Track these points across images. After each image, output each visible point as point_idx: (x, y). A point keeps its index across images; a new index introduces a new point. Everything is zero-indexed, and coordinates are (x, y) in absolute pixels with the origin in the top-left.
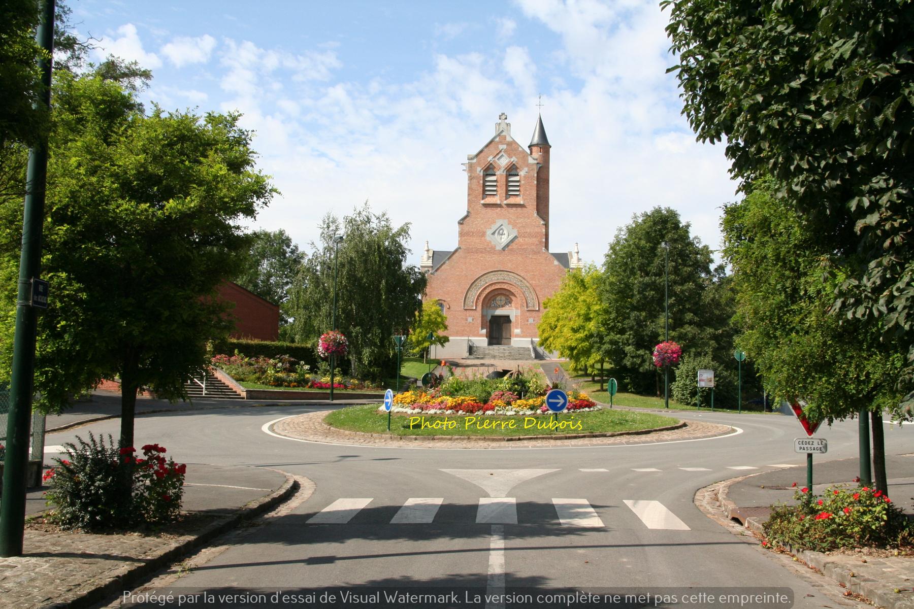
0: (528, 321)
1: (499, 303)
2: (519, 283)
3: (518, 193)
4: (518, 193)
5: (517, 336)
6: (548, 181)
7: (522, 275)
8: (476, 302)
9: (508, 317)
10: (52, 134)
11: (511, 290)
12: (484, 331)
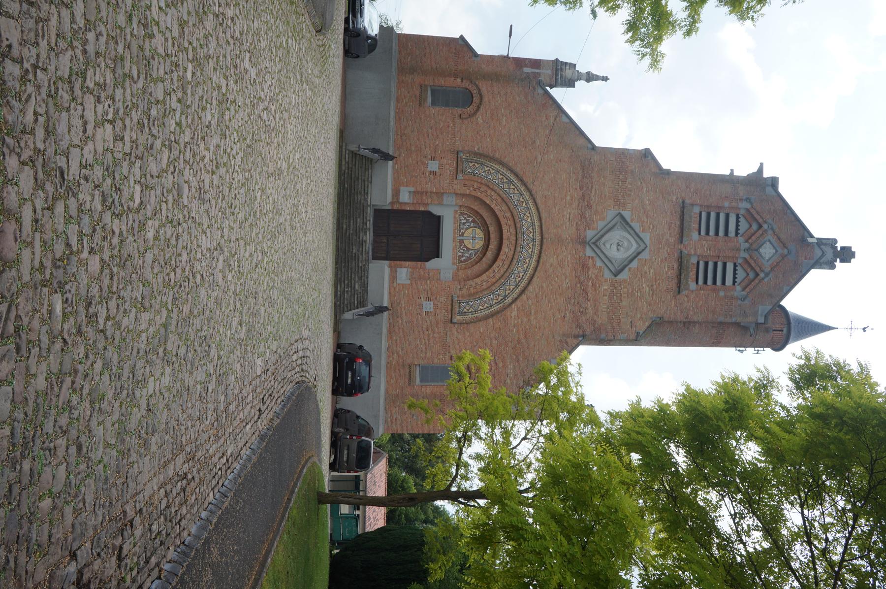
0: (428, 299)
1: (469, 233)
2: (512, 281)
3: (703, 232)
4: (703, 232)
5: (393, 277)
6: (716, 346)
7: (531, 288)
8: (477, 198)
9: (437, 254)
10: (708, 405)
11: (499, 263)
12: (405, 197)
